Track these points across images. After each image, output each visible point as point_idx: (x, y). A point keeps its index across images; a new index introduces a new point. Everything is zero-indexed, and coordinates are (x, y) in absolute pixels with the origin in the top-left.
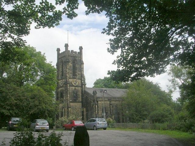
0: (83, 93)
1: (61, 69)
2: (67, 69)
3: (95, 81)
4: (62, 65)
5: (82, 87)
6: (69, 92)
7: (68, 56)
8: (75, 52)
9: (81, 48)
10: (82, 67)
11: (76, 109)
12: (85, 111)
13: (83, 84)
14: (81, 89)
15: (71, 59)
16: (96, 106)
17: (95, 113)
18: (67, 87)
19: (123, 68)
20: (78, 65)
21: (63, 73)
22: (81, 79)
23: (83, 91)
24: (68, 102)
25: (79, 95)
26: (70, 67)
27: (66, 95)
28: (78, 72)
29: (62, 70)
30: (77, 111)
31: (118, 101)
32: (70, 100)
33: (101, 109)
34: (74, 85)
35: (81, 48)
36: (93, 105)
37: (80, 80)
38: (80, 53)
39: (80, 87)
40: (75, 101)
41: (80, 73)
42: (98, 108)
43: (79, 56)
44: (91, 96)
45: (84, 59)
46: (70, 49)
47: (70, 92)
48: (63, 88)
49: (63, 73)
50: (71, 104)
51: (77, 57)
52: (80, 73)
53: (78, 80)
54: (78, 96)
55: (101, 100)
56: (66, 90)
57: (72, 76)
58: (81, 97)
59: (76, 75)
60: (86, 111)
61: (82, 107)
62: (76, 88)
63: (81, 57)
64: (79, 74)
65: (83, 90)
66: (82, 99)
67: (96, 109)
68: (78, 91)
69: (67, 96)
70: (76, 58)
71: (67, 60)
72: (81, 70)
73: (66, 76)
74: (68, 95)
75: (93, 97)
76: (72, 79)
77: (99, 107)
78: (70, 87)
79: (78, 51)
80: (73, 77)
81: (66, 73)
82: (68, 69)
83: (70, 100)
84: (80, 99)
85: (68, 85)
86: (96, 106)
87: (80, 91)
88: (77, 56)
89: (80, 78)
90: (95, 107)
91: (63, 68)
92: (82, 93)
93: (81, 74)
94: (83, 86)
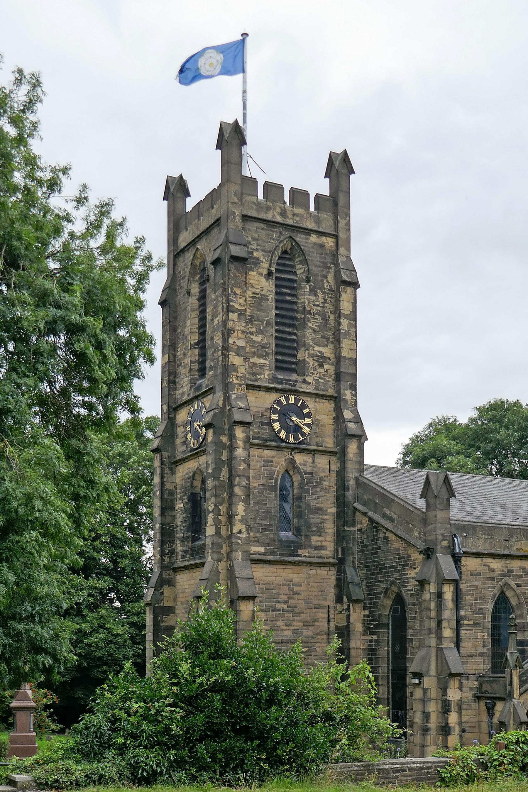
0: (350, 495)
1: (190, 324)
2: (233, 316)
3: (484, 401)
4: (203, 297)
5: (341, 454)
6: (248, 488)
7: (245, 218)
8: (299, 196)
9: (339, 168)
10: (345, 307)
11: (291, 609)
12: (358, 627)
13: (350, 435)
14: (335, 466)
15: (263, 245)
16: (448, 591)
17: (433, 642)
18: (232, 449)
19: (185, 443)
20: (313, 291)
21: (203, 355)
22: (337, 399)
23: (352, 483)
24: (238, 556)
25: (319, 510)
26: (259, 300)
27: (223, 508)
28: (313, 347)
29: (203, 333)
30: (297, 625)
31: (202, 327)
32: (249, 542)
33: (478, 618)
34: (283, 434)
35: (339, 168)
36: (422, 583)
37: (328, 406)
38: (337, 203)
39: (333, 565)
40: (286, 554)
41: (328, 351)
42: (458, 607)
43: (327, 226)
44: (408, 512)
45: (362, 253)
46: (262, 164)
47: (254, 484)
48: (203, 459)
49: (203, 355)
50: (261, 573)
51: (308, 232)
52: (328, 351)
53: (310, 402)
54: (314, 519)
55: (481, 549)
56: (225, 472)
57: (267, 374)
58: (330, 528)
59: (299, 368)
60: (368, 631)
61: (339, 600)
62: (299, 458)
63: (342, 235)
64: (322, 360)
65: (351, 475)
66: (340, 537)
67: (448, 614)
68: (311, 480)
69: (230, 517)
70: (300, 238)
71: (235, 250)
72: (340, 327)
73: (227, 369)
74: (240, 509)
75: (425, 522)
76: (269, 390)
77: (468, 599)
78: (255, 452)
79: (323, 187)
80: (275, 379)
81: (226, 348)
82: (241, 314)
83: (249, 542)
84: (326, 543)
85: (239, 433)
86: (448, 591)
87: (331, 482)
88: (310, 225)
89: (331, 392)
90: (439, 595)
91: (209, 318)
92: (341, 502)
93: (339, 359)
94: (352, 447)
